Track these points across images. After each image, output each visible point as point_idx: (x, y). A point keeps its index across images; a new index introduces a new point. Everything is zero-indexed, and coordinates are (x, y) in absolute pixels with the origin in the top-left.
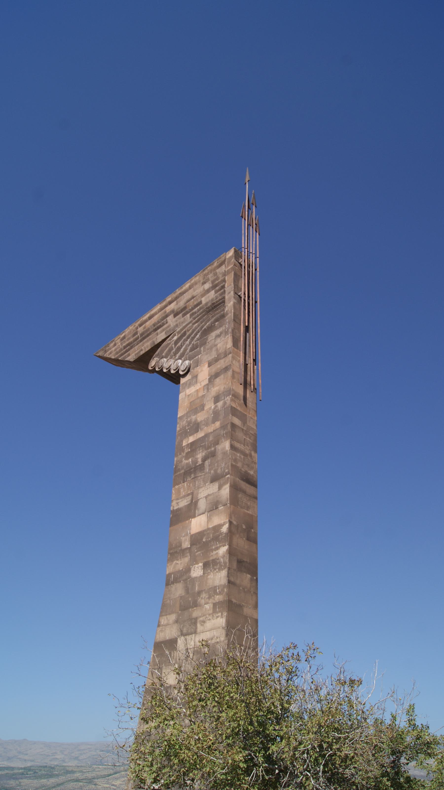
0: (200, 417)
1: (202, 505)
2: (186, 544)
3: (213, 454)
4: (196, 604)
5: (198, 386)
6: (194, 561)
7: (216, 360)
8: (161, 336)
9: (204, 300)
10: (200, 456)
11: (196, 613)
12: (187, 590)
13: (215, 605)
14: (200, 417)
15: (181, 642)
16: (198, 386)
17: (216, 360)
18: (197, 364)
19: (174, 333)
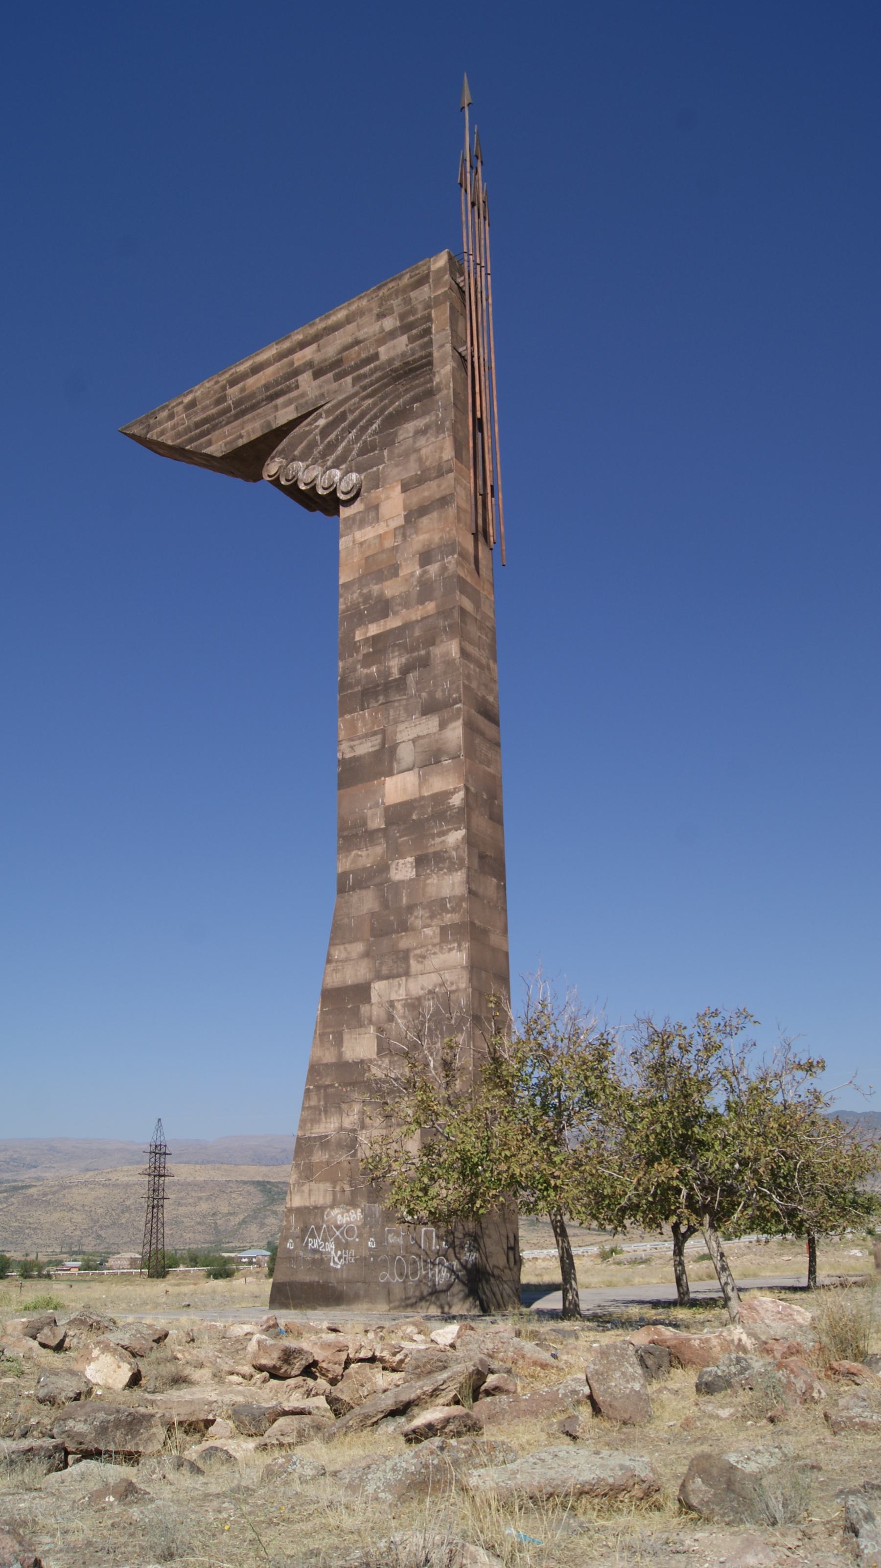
0: (391, 589)
1: (406, 753)
2: (377, 822)
3: (425, 663)
4: (404, 927)
5: (381, 528)
6: (396, 852)
7: (420, 480)
8: (285, 415)
9: (385, 353)
10: (395, 663)
11: (405, 942)
12: (385, 904)
13: (443, 930)
14: (391, 589)
15: (378, 988)
16: (381, 528)
17: (420, 480)
18: (376, 482)
19: (318, 411)
